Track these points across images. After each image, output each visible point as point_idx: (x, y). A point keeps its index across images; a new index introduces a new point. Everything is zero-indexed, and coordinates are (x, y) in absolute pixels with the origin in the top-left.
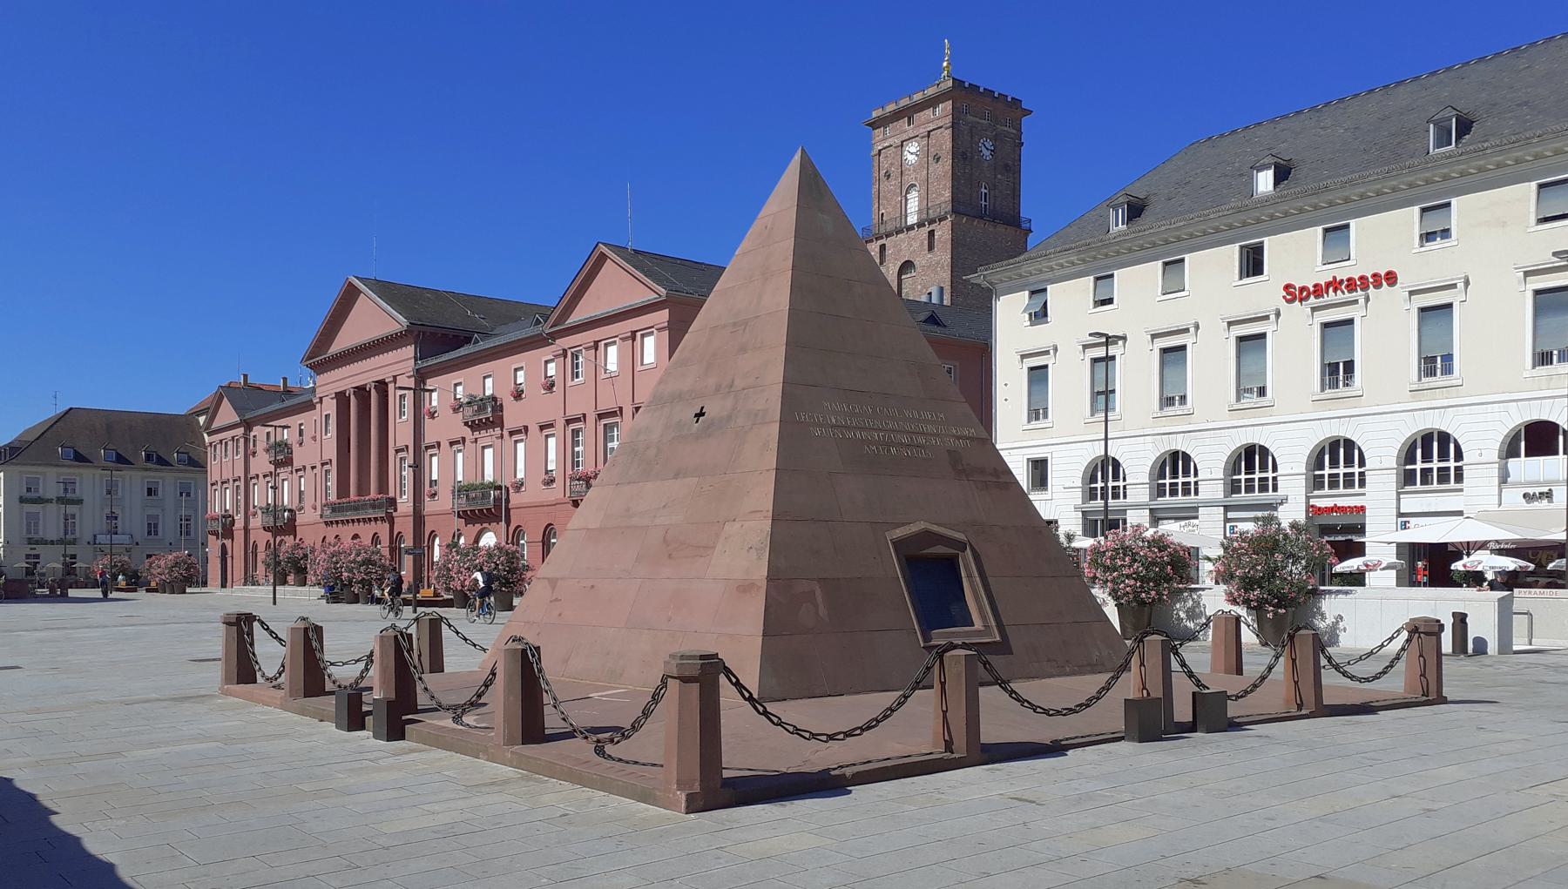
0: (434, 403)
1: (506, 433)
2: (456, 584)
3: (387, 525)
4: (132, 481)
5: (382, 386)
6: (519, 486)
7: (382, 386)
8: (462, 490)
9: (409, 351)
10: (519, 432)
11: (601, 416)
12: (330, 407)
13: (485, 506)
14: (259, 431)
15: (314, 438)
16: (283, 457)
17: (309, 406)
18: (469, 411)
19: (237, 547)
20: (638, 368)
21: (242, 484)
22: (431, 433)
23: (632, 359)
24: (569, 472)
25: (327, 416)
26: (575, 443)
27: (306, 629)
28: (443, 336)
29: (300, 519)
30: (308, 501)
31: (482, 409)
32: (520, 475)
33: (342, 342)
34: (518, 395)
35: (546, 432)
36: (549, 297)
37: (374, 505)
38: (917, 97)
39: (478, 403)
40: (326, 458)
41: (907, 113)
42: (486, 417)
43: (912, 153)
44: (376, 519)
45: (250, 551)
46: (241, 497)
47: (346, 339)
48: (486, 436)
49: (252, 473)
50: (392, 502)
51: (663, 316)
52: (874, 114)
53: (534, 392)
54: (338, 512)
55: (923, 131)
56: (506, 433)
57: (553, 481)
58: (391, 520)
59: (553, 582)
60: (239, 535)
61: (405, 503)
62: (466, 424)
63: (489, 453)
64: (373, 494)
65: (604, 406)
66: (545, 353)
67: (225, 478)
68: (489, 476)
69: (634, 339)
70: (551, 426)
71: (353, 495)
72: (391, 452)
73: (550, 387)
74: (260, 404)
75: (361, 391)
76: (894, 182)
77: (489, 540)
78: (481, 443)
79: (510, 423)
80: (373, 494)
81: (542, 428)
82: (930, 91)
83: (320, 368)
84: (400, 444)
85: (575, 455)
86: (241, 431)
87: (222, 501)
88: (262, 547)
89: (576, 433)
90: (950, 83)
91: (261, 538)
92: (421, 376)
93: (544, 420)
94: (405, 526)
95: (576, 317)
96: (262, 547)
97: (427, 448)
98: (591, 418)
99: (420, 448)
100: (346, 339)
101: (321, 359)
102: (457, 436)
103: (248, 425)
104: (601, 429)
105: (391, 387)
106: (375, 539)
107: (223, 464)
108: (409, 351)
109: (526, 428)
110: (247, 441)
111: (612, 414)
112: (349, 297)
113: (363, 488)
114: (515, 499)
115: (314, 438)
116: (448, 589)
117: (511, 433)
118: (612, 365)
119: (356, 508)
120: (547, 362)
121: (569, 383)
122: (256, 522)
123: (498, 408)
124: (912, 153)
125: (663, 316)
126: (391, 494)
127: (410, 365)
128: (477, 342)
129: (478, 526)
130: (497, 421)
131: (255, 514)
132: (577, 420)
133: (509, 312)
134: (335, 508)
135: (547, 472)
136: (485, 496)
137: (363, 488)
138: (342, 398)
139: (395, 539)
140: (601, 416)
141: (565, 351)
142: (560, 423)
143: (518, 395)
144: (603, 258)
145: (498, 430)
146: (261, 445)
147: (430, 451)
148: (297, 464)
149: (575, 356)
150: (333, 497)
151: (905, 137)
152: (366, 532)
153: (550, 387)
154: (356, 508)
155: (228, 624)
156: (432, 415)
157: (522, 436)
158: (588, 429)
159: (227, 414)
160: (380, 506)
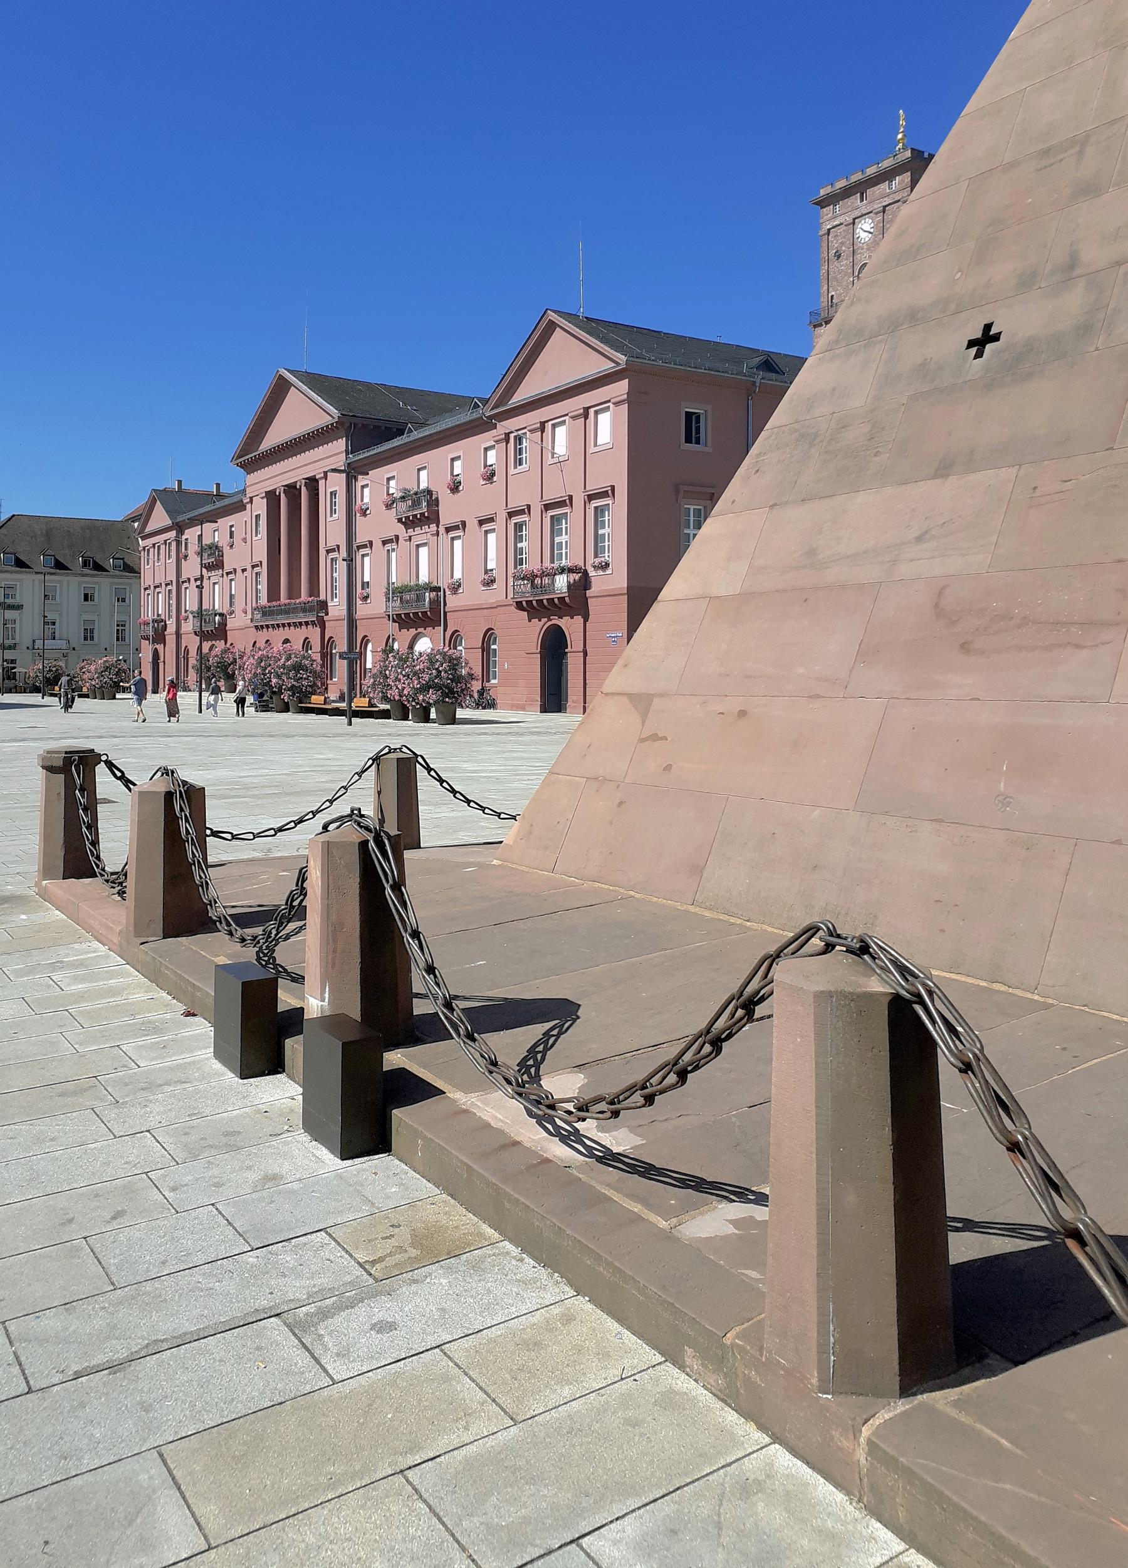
0: (366, 500)
1: (442, 530)
2: (394, 693)
3: (318, 629)
4: (69, 587)
5: (312, 483)
6: (456, 588)
7: (312, 483)
8: (397, 592)
9: (341, 444)
10: (456, 528)
11: (547, 507)
12: (260, 507)
13: (422, 610)
14: (191, 534)
15: (245, 540)
16: (213, 558)
17: (239, 507)
18: (402, 507)
19: (168, 652)
20: (591, 449)
21: (174, 588)
22: (364, 530)
23: (585, 440)
24: (511, 569)
25: (333, 494)
26: (598, 524)
27: (169, 796)
28: (375, 427)
29: (231, 624)
30: (239, 605)
31: (416, 504)
32: (458, 575)
33: (274, 437)
34: (455, 488)
35: (486, 527)
36: (477, 382)
37: (305, 608)
38: (871, 171)
39: (413, 497)
40: (256, 560)
41: (860, 188)
42: (421, 512)
43: (865, 229)
44: (307, 623)
45: (182, 656)
46: (173, 602)
47: (277, 435)
48: (422, 534)
49: (184, 577)
50: (323, 605)
51: (621, 388)
52: (823, 192)
53: (473, 483)
54: (269, 615)
55: (878, 206)
56: (442, 530)
57: (493, 581)
58: (322, 624)
59: (642, 702)
60: (171, 640)
61: (337, 607)
62: (400, 520)
63: (424, 552)
64: (304, 597)
65: (551, 495)
66: (486, 439)
67: (157, 582)
68: (424, 578)
69: (543, 431)
70: (491, 520)
71: (284, 599)
72: (322, 552)
73: (490, 477)
74: (190, 508)
75: (292, 490)
76: (845, 262)
77: (424, 645)
78: (416, 541)
79: (446, 519)
80: (304, 597)
81: (481, 523)
82: (887, 163)
83: (250, 466)
84: (331, 544)
85: (518, 552)
86: (173, 534)
87: (154, 605)
88: (193, 653)
89: (519, 527)
90: (908, 154)
91: (191, 642)
92: (352, 472)
93: (484, 513)
94: (338, 632)
95: (521, 395)
96: (193, 653)
97: (359, 548)
98: (536, 509)
99: (353, 550)
100: (277, 435)
101: (252, 458)
102: (390, 534)
103: (180, 528)
104: (329, 561)
105: (322, 483)
106: (307, 644)
107: (156, 568)
108: (341, 444)
109: (464, 523)
110: (179, 543)
111: (561, 504)
112: (280, 389)
113: (293, 592)
114: (453, 602)
115: (245, 540)
116: (385, 699)
117: (448, 530)
118: (561, 448)
119: (287, 611)
120: (486, 449)
121: (512, 471)
122: (188, 627)
123: (434, 503)
124: (865, 229)
125: (621, 388)
126: (322, 597)
127: (340, 461)
128: (410, 431)
129: (413, 631)
130: (432, 517)
131: (186, 619)
132: (522, 512)
133: (443, 403)
134: (266, 612)
135: (486, 571)
136: (420, 599)
137: (293, 592)
138: (272, 497)
139: (327, 645)
140: (547, 507)
141: (507, 435)
142: (502, 516)
143: (455, 488)
144: (552, 326)
145: (433, 527)
146: (193, 547)
147: (362, 551)
148: (228, 567)
149: (519, 440)
150: (264, 601)
151: (857, 213)
152: (296, 636)
153: (490, 477)
154: (287, 611)
155: (50, 769)
156: (364, 513)
157: (460, 533)
158: (533, 523)
159: (160, 518)
160: (311, 610)
